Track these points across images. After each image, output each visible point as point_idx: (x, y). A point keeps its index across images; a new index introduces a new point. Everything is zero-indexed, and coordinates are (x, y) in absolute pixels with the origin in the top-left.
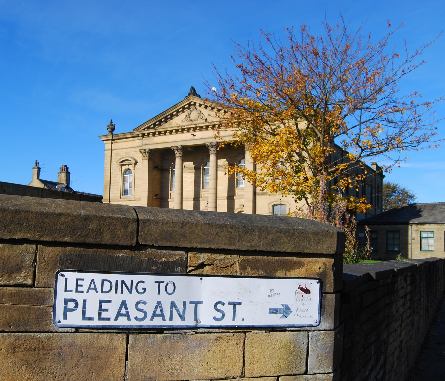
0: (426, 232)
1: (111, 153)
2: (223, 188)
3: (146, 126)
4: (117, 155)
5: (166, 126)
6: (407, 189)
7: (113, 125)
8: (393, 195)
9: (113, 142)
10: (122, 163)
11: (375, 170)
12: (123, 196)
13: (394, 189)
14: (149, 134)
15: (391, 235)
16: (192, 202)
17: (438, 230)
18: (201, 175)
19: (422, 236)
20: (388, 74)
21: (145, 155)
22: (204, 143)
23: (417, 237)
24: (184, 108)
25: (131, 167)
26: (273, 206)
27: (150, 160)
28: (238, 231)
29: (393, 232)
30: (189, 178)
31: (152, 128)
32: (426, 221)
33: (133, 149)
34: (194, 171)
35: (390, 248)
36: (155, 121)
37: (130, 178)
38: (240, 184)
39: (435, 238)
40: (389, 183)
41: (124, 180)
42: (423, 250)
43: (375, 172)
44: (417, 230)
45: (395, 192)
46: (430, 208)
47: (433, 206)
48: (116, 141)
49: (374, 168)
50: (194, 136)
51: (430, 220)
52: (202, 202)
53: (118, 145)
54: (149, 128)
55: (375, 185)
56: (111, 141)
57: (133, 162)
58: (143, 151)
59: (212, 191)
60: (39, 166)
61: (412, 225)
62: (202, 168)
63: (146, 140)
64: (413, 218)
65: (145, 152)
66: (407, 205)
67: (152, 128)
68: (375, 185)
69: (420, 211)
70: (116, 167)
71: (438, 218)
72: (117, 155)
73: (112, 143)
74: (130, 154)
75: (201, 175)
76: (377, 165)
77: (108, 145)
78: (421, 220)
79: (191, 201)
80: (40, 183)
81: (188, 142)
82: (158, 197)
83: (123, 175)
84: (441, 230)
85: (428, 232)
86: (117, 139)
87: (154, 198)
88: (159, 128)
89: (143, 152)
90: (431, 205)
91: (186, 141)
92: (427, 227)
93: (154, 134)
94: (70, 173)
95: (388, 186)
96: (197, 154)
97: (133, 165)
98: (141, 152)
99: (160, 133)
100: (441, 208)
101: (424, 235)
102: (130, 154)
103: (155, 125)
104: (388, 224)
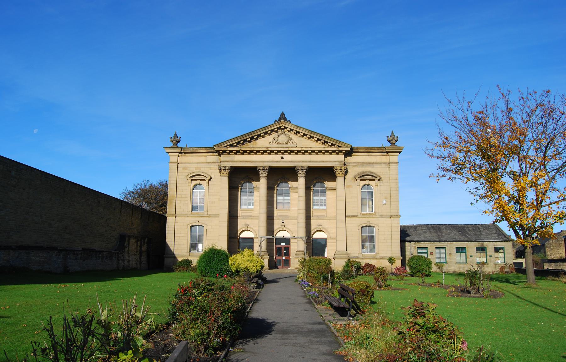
3: (229, 144)
5: (248, 146)
17: (430, 246)
24: (273, 131)
26: (192, 226)
28: (258, 255)
44: (415, 247)
48: (183, 154)
50: (282, 158)
54: (231, 146)
62: (276, 188)
72: (185, 169)
75: (239, 192)
81: (275, 163)
84: (433, 246)
86: (185, 153)
96: (280, 176)
103: (238, 143)
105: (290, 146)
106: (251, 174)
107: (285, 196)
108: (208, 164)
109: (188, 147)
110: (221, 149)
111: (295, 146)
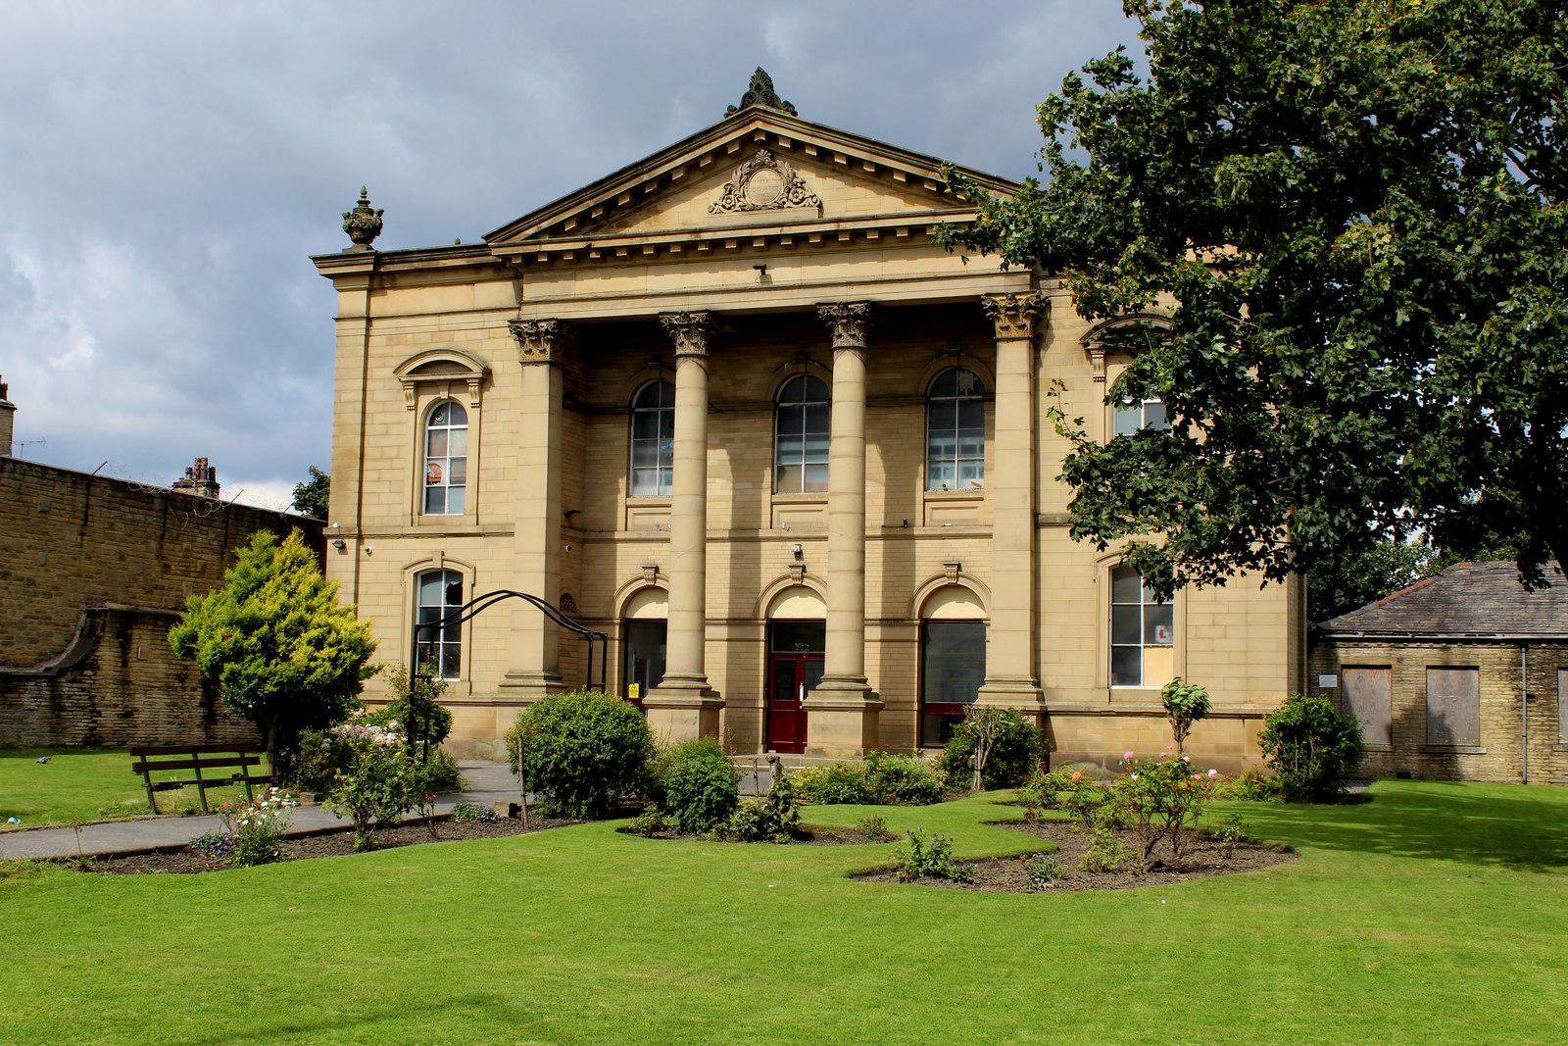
3: (544, 225)
7: (371, 212)
12: (420, 514)
22: (656, 311)
25: (465, 399)
31: (571, 232)
36: (591, 203)
54: (556, 231)
67: (571, 232)
72: (393, 339)
88: (628, 231)
89: (525, 334)
103: (583, 219)
105: (797, 216)
106: (646, 341)
107: (808, 439)
108: (473, 320)
109: (462, 244)
110: (516, 250)
111: (813, 214)
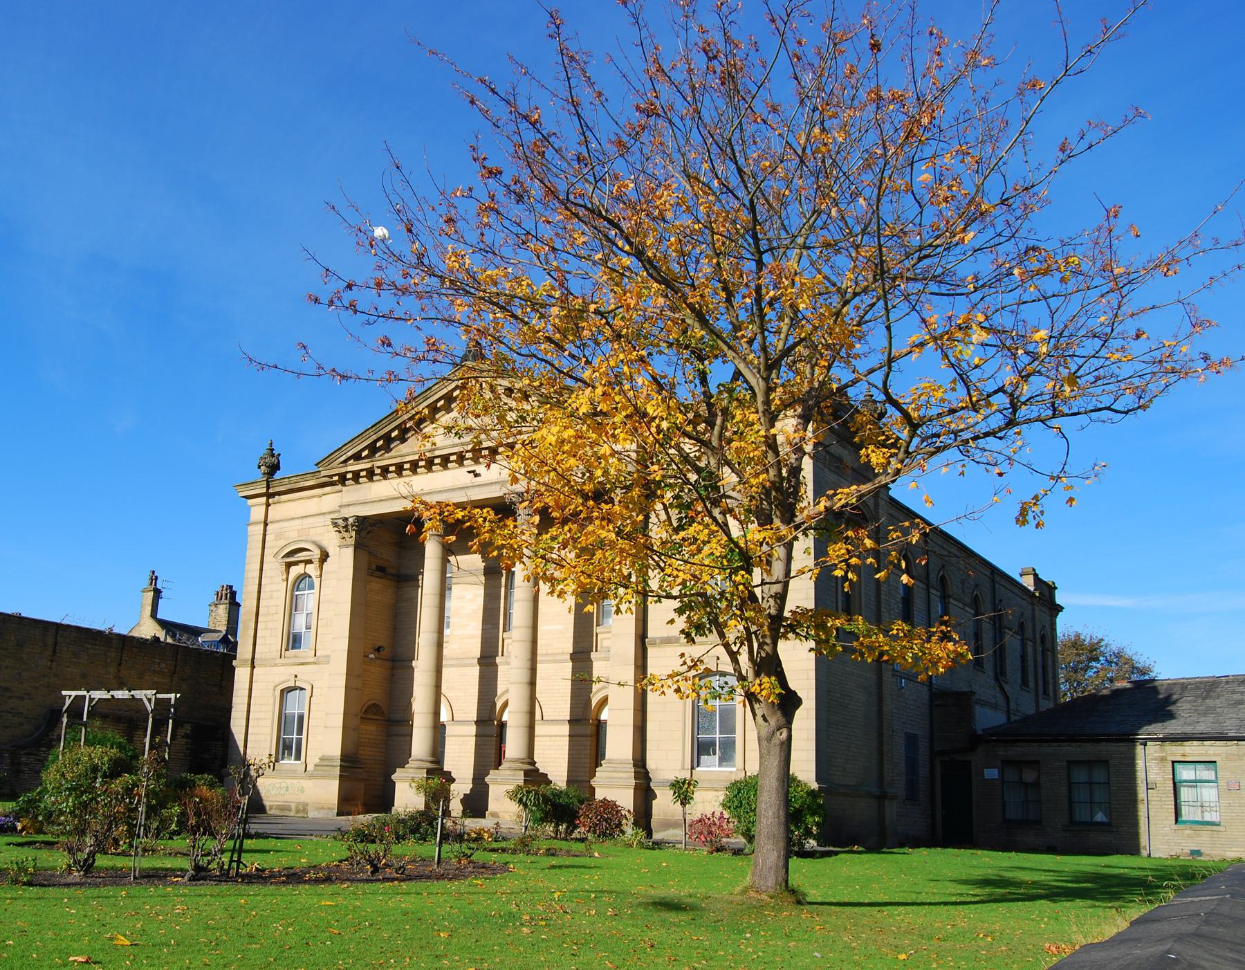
0: (1192, 766)
1: (265, 530)
2: (561, 627)
3: (350, 454)
4: (278, 536)
6: (1129, 652)
8: (1092, 668)
9: (271, 501)
10: (292, 557)
11: (1032, 588)
13: (1092, 651)
14: (356, 476)
15: (1080, 775)
16: (476, 670)
18: (503, 590)
19: (1178, 778)
20: (1016, 170)
21: (346, 535)
23: (1164, 779)
25: (312, 569)
27: (358, 547)
29: (1090, 764)
30: (467, 600)
31: (366, 457)
32: (1188, 729)
33: (313, 518)
34: (483, 578)
35: (1081, 814)
36: (375, 437)
37: (309, 599)
38: (609, 615)
39: (1222, 783)
40: (1078, 636)
41: (293, 605)
42: (1185, 822)
43: (1031, 595)
44: (1163, 759)
45: (1097, 660)
46: (1199, 692)
47: (1209, 688)
49: (1028, 582)
50: (476, 475)
51: (1201, 728)
52: (501, 670)
53: (284, 508)
54: (357, 457)
55: (1034, 631)
56: (264, 499)
57: (317, 554)
58: (340, 522)
59: (525, 634)
60: (159, 587)
61: (1145, 745)
63: (350, 493)
64: (1150, 723)
65: (346, 527)
66: (1129, 686)
67: (366, 457)
68: (1034, 631)
69: (1168, 701)
70: (274, 567)
71: (1228, 723)
73: (268, 505)
74: (312, 532)
75: (503, 590)
76: (1036, 575)
77: (257, 510)
78: (1172, 727)
79: (472, 665)
80: (158, 628)
82: (384, 653)
83: (292, 591)
85: (1198, 766)
86: (280, 494)
87: (372, 656)
89: (342, 525)
90: (1201, 683)
91: (454, 490)
92: (1193, 750)
93: (370, 474)
94: (239, 605)
95: (1076, 643)
97: (317, 563)
98: (335, 525)
99: (385, 471)
100: (1234, 692)
101: (1185, 773)
102: (312, 532)
103: (373, 449)
104: (1071, 739)
